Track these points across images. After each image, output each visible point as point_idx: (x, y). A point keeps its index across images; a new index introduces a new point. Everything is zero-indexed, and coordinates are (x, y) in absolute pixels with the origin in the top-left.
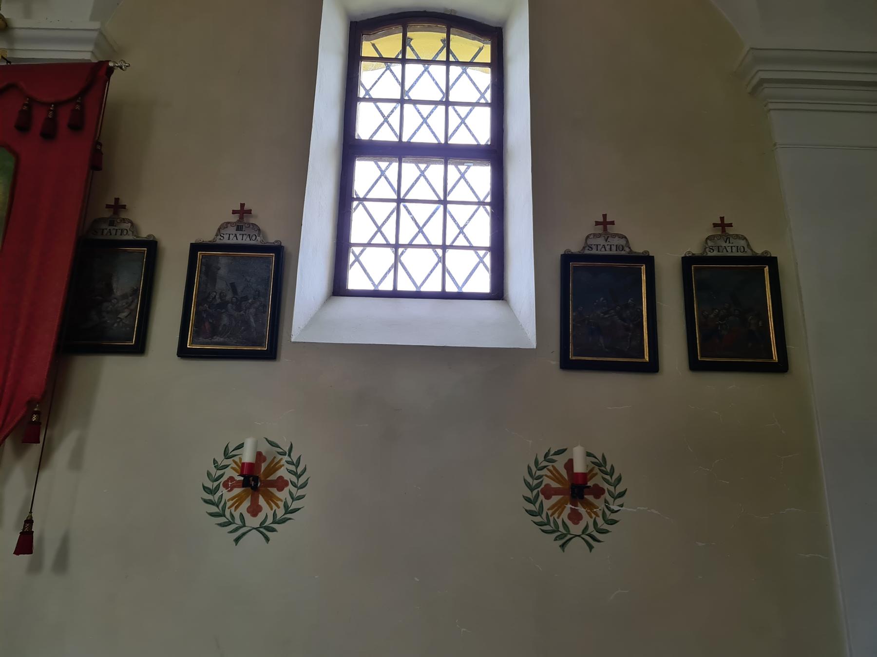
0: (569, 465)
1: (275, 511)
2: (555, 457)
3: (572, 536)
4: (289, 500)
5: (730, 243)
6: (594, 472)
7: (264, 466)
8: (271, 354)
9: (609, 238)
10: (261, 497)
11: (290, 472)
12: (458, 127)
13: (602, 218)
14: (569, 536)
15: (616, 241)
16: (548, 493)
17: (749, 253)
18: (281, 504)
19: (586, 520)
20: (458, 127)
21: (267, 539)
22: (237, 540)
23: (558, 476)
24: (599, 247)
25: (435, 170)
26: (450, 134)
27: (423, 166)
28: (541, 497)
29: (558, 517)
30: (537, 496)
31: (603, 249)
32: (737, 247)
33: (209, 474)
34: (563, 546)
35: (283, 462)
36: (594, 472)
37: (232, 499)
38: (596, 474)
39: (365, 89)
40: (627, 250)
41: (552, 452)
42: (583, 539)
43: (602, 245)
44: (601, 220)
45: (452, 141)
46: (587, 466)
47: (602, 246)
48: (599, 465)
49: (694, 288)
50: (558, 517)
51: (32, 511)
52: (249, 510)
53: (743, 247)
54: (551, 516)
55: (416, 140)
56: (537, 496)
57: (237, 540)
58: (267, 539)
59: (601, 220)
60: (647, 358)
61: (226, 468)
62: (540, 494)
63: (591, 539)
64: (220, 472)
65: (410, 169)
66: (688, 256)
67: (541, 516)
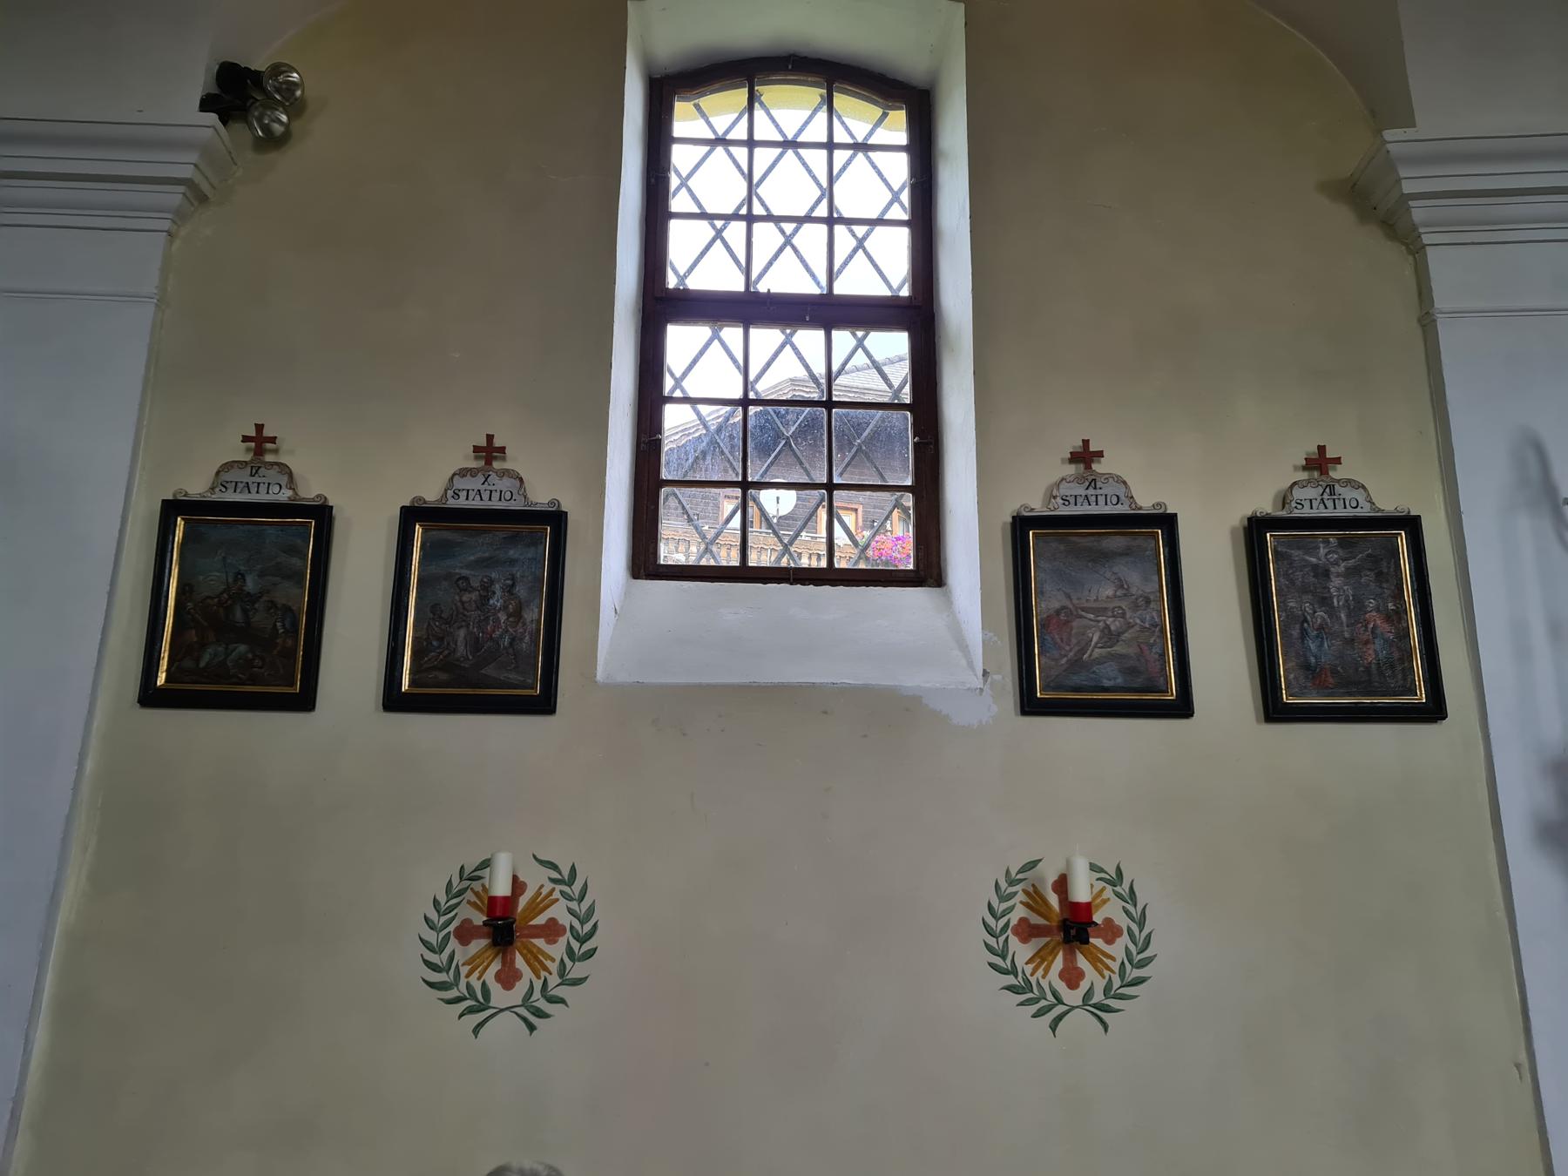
0: (1062, 885)
1: (545, 980)
3: (495, 1011)
5: (1095, 488)
6: (553, 897)
7: (523, 901)
9: (262, 469)
10: (518, 955)
11: (571, 911)
12: (851, 257)
13: (254, 432)
14: (1060, 1009)
15: (505, 484)
19: (1091, 975)
20: (851, 257)
22: (476, 1030)
23: (537, 910)
24: (472, 494)
25: (810, 340)
26: (836, 268)
27: (860, 334)
28: (453, 944)
29: (1044, 977)
30: (446, 938)
31: (478, 497)
32: (501, 492)
33: (436, 903)
35: (557, 895)
36: (553, 897)
38: (557, 900)
39: (679, 175)
40: (289, 493)
42: (525, 1020)
43: (476, 491)
45: (839, 289)
46: (1092, 886)
47: (1309, 503)
48: (1112, 883)
49: (1272, 574)
50: (1044, 977)
52: (499, 977)
53: (1118, 496)
54: (1032, 975)
55: (695, 283)
56: (446, 938)
57: (476, 1030)
59: (483, 443)
61: (1012, 911)
62: (452, 936)
64: (1004, 920)
65: (765, 339)
66: (416, 505)
67: (448, 973)
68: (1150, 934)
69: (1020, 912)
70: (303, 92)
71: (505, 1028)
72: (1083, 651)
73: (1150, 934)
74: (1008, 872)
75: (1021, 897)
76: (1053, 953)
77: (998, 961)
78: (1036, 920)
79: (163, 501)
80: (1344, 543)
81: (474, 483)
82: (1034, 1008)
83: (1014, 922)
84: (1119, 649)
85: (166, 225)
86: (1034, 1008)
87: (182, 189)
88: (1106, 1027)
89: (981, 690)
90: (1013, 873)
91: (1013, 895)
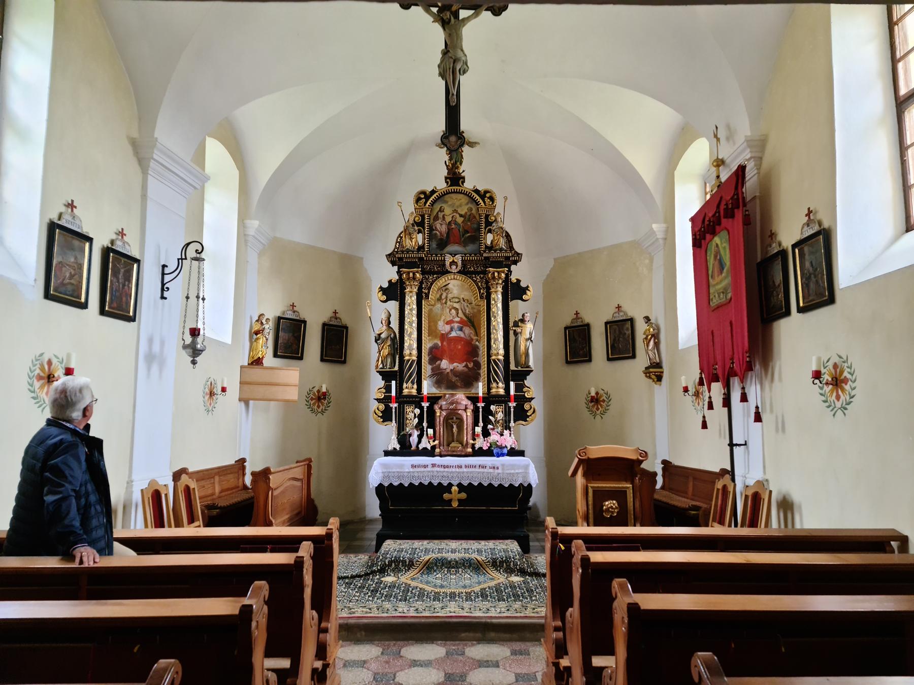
2: (827, 364)
4: (850, 390)
8: (831, 300)
16: (312, 399)
17: (340, 324)
18: (847, 393)
21: (602, 418)
28: (310, 401)
34: (316, 415)
35: (845, 367)
37: (844, 395)
41: (825, 362)
44: (295, 305)
47: (289, 315)
51: (728, 448)
58: (602, 418)
59: (292, 304)
60: (300, 355)
63: (322, 412)
68: (852, 402)
69: (38, 371)
70: (468, 19)
71: (598, 417)
72: (64, 280)
73: (852, 402)
74: (35, 357)
75: (38, 366)
76: (45, 386)
77: (30, 388)
78: (42, 374)
79: (322, 360)
80: (617, 325)
81: (617, 315)
82: (38, 405)
83: (36, 375)
84: (72, 281)
85: (756, 172)
86: (38, 405)
87: (753, 160)
88: (845, 414)
89: (34, 286)
90: (37, 357)
91: (36, 364)
